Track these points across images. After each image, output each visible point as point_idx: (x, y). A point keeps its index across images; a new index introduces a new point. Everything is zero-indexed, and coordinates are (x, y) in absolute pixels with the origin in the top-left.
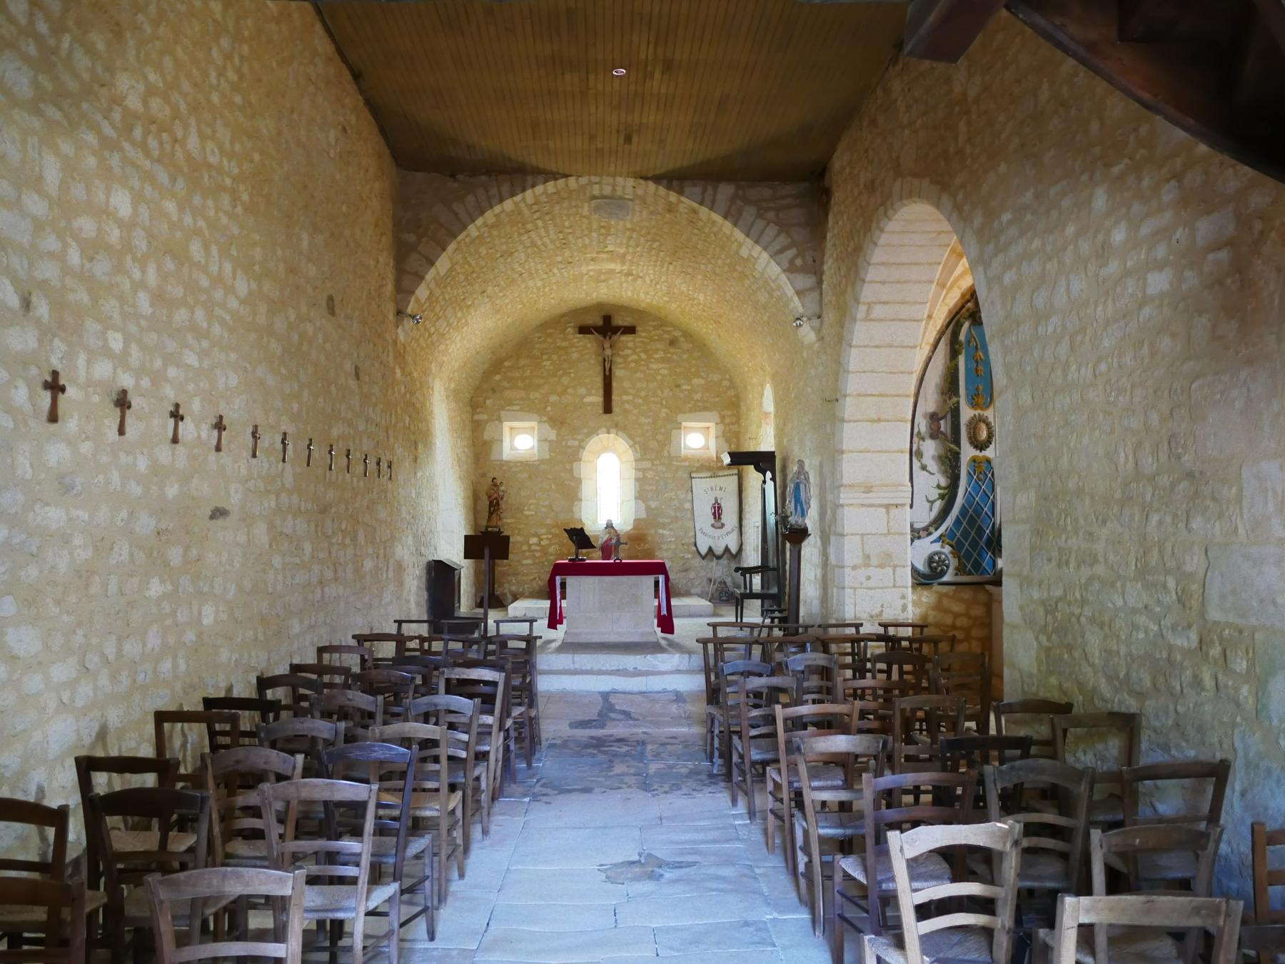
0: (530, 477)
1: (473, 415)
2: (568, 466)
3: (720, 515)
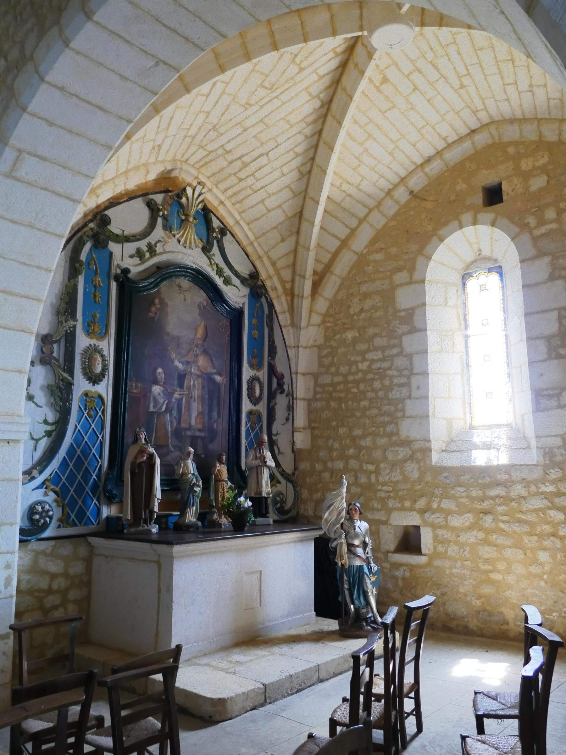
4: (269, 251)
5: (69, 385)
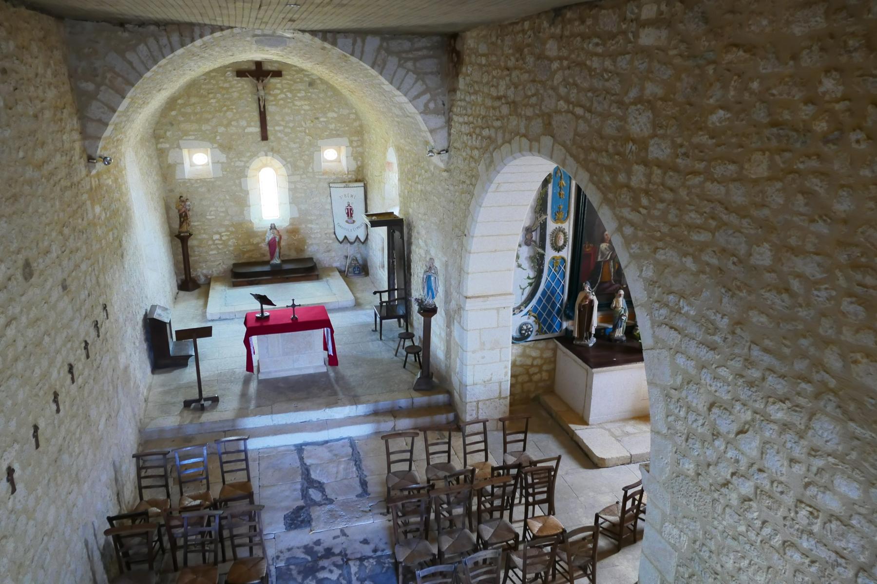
0: (209, 190)
1: (157, 144)
2: (237, 181)
3: (351, 214)
5: (542, 256)
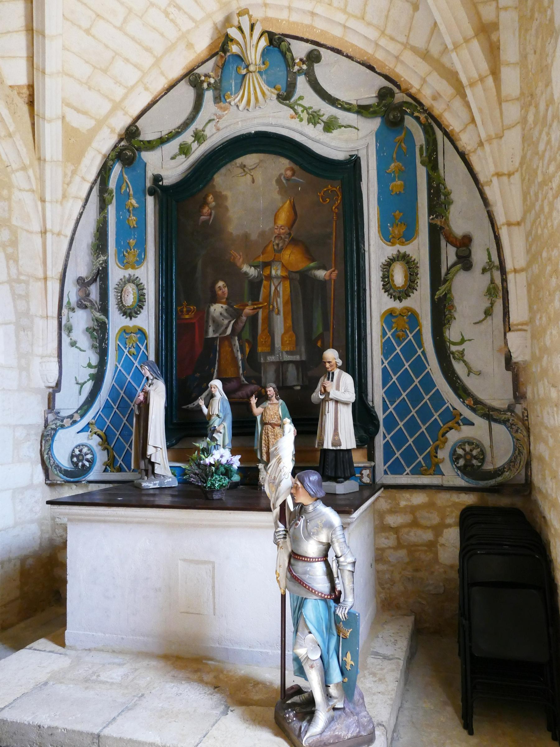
4: (408, 39)
